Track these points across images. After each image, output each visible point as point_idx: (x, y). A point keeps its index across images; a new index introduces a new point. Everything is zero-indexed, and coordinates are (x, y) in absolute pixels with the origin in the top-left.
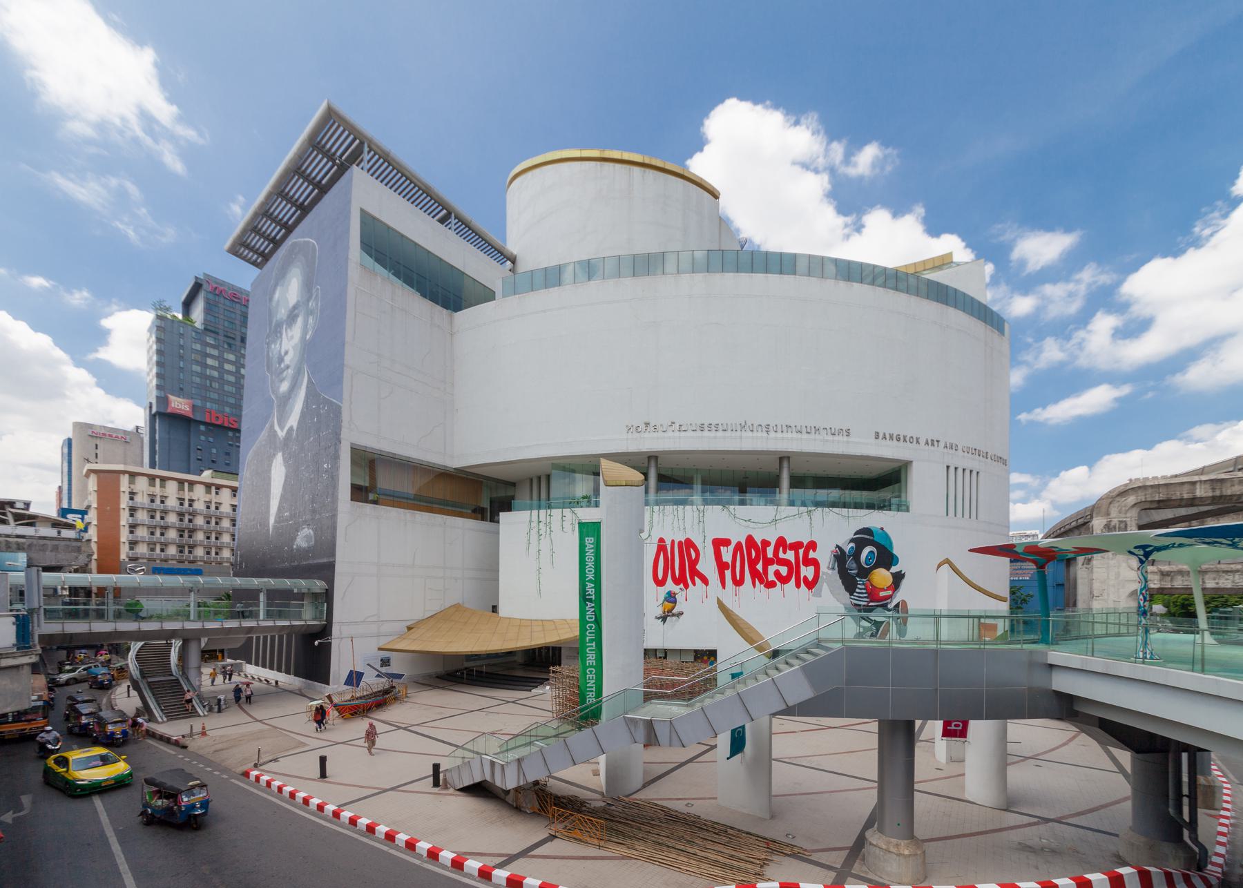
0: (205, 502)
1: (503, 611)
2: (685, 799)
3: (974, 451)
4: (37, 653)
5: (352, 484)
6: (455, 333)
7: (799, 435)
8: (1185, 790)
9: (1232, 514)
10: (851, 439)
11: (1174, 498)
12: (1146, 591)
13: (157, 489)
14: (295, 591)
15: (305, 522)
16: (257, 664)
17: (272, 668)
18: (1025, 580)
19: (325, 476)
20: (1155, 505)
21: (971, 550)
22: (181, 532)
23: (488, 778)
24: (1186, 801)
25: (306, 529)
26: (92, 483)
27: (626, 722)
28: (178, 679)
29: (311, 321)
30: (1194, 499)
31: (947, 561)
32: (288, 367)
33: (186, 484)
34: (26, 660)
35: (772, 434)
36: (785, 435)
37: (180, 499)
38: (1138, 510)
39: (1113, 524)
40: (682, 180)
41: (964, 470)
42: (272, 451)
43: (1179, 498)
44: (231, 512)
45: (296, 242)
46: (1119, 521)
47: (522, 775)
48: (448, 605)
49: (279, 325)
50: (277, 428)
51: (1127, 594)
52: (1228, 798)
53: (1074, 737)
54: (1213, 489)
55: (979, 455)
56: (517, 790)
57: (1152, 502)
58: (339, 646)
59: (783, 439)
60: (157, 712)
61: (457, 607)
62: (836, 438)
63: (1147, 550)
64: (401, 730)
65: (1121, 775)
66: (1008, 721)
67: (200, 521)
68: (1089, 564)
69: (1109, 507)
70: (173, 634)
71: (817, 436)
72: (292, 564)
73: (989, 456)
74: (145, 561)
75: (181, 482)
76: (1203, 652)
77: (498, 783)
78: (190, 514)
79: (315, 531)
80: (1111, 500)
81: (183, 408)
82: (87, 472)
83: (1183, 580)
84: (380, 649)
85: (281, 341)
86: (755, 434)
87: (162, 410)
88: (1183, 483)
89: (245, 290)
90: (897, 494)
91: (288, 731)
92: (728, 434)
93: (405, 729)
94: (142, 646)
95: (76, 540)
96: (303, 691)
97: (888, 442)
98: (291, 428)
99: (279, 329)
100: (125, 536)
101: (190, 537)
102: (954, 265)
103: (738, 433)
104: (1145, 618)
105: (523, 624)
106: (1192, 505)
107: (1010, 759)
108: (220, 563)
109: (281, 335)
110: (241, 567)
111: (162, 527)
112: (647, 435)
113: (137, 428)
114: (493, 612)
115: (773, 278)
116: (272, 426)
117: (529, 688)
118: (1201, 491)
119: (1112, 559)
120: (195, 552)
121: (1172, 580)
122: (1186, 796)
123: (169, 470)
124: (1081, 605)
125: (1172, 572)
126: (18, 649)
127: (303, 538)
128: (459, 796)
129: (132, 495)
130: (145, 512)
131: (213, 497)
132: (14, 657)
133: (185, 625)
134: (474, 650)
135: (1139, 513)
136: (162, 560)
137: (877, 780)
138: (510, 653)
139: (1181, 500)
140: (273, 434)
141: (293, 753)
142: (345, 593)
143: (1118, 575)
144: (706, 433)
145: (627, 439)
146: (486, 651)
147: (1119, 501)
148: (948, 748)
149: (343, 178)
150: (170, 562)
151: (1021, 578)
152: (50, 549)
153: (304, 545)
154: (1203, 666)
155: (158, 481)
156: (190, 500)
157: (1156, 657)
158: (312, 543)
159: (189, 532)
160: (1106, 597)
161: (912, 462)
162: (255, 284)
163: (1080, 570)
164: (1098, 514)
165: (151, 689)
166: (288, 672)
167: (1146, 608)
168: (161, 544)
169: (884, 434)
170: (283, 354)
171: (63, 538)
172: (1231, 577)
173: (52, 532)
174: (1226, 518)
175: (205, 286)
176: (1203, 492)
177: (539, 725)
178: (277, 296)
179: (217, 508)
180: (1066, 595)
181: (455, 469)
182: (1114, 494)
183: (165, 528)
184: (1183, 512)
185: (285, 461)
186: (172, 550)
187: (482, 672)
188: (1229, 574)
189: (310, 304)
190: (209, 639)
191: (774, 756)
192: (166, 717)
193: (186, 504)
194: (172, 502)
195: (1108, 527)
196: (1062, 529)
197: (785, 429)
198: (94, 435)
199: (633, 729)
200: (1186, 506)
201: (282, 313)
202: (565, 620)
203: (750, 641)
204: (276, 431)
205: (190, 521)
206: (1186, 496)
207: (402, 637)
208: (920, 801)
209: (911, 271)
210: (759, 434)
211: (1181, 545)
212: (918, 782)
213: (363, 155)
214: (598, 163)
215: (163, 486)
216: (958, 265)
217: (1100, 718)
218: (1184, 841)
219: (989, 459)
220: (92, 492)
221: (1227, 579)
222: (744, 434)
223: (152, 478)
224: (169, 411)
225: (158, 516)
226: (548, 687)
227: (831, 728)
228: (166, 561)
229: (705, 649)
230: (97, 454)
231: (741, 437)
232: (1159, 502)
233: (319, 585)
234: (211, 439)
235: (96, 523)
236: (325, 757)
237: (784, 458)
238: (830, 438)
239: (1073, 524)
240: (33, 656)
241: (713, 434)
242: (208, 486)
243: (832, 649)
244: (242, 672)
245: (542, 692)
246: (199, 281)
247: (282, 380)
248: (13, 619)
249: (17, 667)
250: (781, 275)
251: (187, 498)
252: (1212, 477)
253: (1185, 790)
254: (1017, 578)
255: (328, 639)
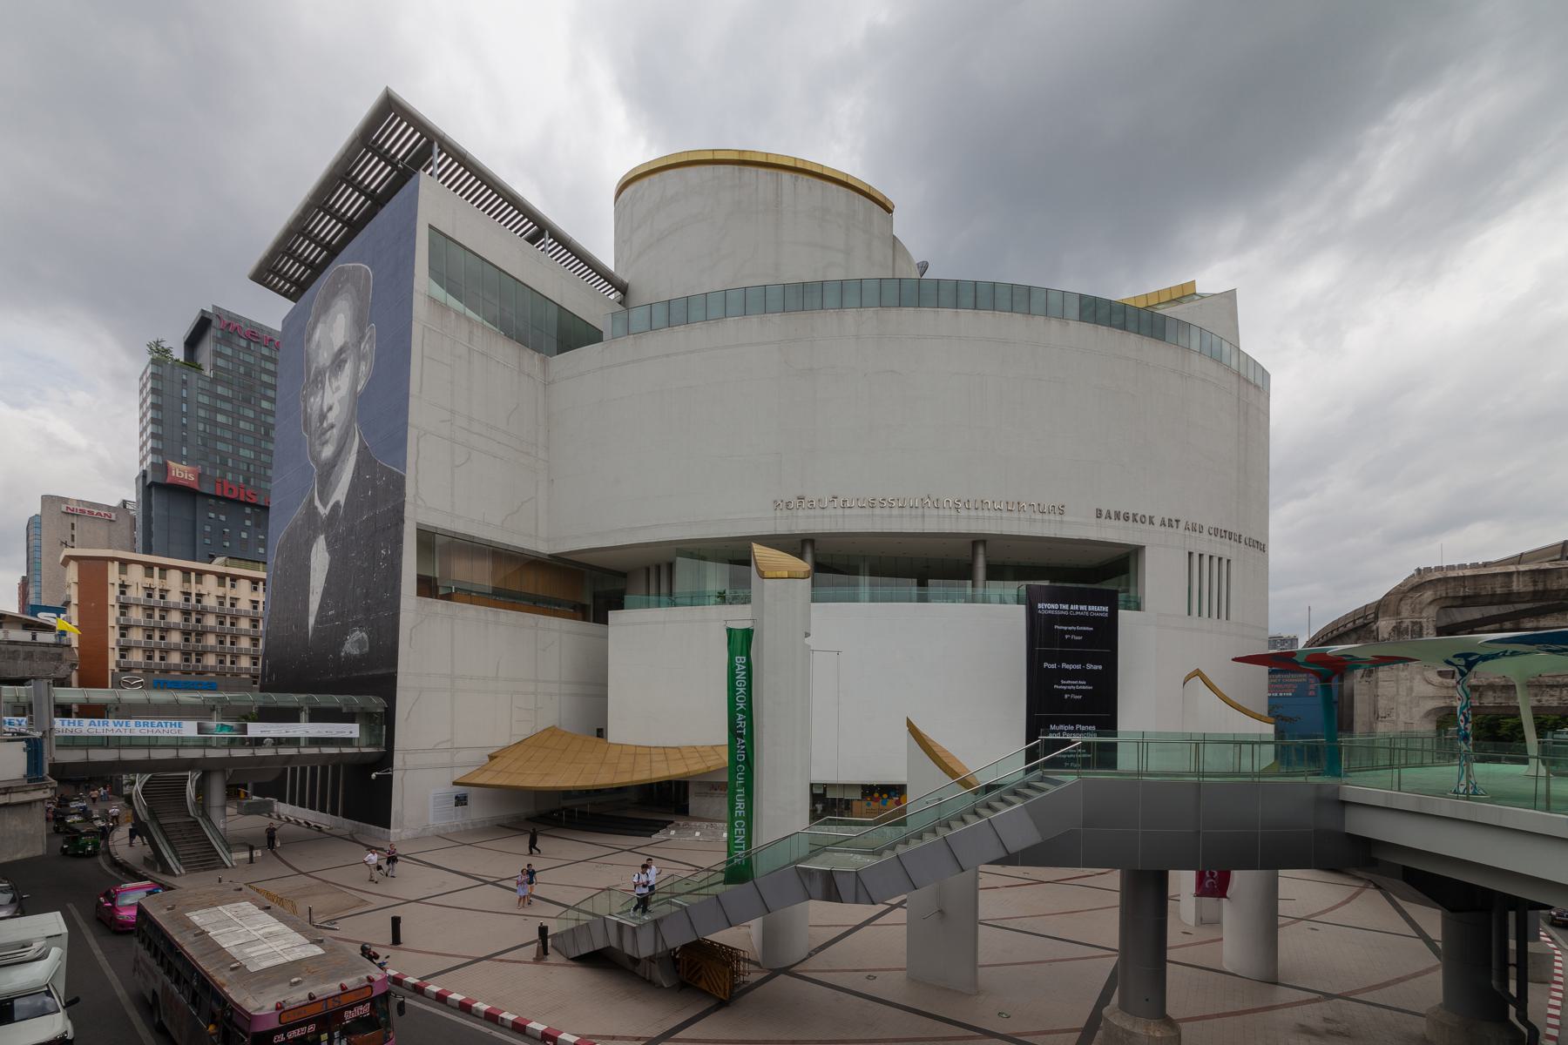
0: (218, 597)
1: (614, 735)
2: (865, 970)
3: (1223, 534)
4: (53, 786)
5: (418, 575)
6: (549, 383)
7: (999, 513)
8: (1513, 959)
9: (1556, 614)
10: (1066, 518)
11: (1483, 593)
12: (1468, 710)
13: (156, 582)
14: (344, 710)
15: (356, 623)
16: (292, 802)
17: (312, 807)
18: (1286, 696)
19: (383, 565)
20: (1459, 602)
21: (1236, 660)
22: (186, 634)
23: (614, 944)
24: (1513, 971)
25: (358, 632)
26: (72, 573)
27: (799, 874)
28: (197, 821)
29: (363, 368)
30: (1510, 594)
31: (1198, 673)
32: (332, 426)
33: (193, 575)
34: (39, 795)
35: (963, 512)
36: (980, 513)
37: (184, 593)
38: (1438, 608)
39: (1404, 625)
40: (846, 189)
41: (1211, 557)
42: (311, 532)
43: (1490, 593)
44: (251, 610)
45: (343, 267)
46: (1412, 622)
47: (660, 942)
48: (540, 728)
49: (320, 373)
50: (317, 503)
51: (1422, 714)
52: (1560, 972)
53: (1357, 894)
54: (1535, 583)
55: (1230, 539)
56: (651, 959)
57: (1455, 598)
58: (402, 779)
59: (977, 518)
60: (172, 862)
61: (552, 731)
62: (1046, 517)
63: (1470, 659)
64: (489, 886)
65: (1432, 938)
66: (1281, 872)
67: (211, 621)
68: (1370, 677)
69: (1399, 605)
70: (191, 764)
71: (1022, 515)
72: (340, 676)
73: (1243, 540)
74: (140, 672)
75: (186, 572)
76: (1548, 791)
77: (628, 950)
78: (198, 612)
79: (369, 634)
80: (1401, 596)
81: (186, 478)
82: (64, 559)
83: (1495, 697)
84: (455, 783)
85: (324, 393)
86: (941, 512)
87: (159, 480)
88: (1495, 575)
89: (266, 327)
90: (1124, 588)
91: (344, 886)
92: (906, 511)
93: (494, 884)
94: (149, 780)
95: (55, 645)
96: (355, 836)
97: (1113, 522)
98: (337, 503)
99: (319, 379)
100: (113, 637)
101: (198, 641)
102: (1197, 298)
103: (920, 511)
104: (1466, 744)
105: (638, 753)
106: (1507, 602)
107: (1281, 921)
108: (237, 675)
109: (323, 388)
110: (270, 680)
111: (162, 630)
112: (800, 513)
113: (124, 503)
114: (598, 736)
115: (966, 315)
116: (311, 501)
117: (649, 833)
118: (1518, 585)
119: (1403, 670)
120: (130, 656)
121: (1480, 697)
122: (1513, 965)
123: (168, 556)
124: (1359, 726)
125: (1479, 686)
126: (29, 781)
127: (355, 643)
128: (574, 966)
129: (124, 587)
130: (140, 609)
131: (229, 592)
132: (26, 792)
133: (232, 753)
134: (576, 785)
135: (1438, 611)
136: (162, 671)
137: (1117, 948)
138: (621, 790)
139: (1494, 595)
140: (312, 511)
141: (349, 914)
142: (409, 714)
143: (1411, 689)
144: (878, 511)
145: (775, 518)
146: (593, 786)
147: (1412, 597)
148: (1198, 908)
149: (405, 186)
150: (173, 673)
151: (1281, 694)
152: (22, 656)
153: (356, 652)
154: (1548, 802)
155: (156, 570)
156: (161, 590)
157: (1481, 791)
158: (367, 649)
159: (197, 635)
160: (1394, 718)
161: (1144, 547)
162: (287, 322)
163: (1357, 683)
164: (1385, 613)
165: (164, 833)
166: (334, 812)
167: (1468, 732)
168: (161, 650)
169: (1109, 512)
170: (325, 410)
171: (40, 643)
172: (1557, 693)
173: (26, 636)
174: (1548, 618)
175: (215, 322)
176: (1521, 586)
177: (677, 879)
178: (317, 335)
179: (232, 605)
180: (1339, 716)
181: (549, 555)
182: (1406, 588)
183: (166, 630)
184: (1494, 610)
185: (329, 545)
186: (175, 658)
187: (586, 813)
188: (1555, 689)
189: (362, 347)
190: (234, 771)
191: (981, 917)
192: (185, 868)
193: (193, 599)
194: (175, 597)
195: (1398, 630)
196: (1335, 632)
197: (978, 504)
198: (69, 511)
199: (807, 883)
200: (1500, 603)
201: (324, 358)
202: (695, 747)
203: (952, 773)
204: (316, 508)
205: (198, 621)
206: (1499, 591)
207: (482, 769)
208: (1174, 975)
209: (1142, 305)
210: (947, 512)
211: (1514, 654)
212: (1171, 948)
213: (432, 158)
214: (736, 167)
215: (199, 582)
216: (1203, 297)
217: (1404, 866)
218: (1510, 1021)
219: (1243, 542)
220: (72, 585)
221: (1552, 696)
222: (927, 511)
223: (149, 567)
224: (168, 481)
225: (157, 614)
226: (673, 832)
227: (1043, 882)
228: (167, 671)
229: (875, 783)
230: (73, 536)
231: (923, 516)
232: (1464, 598)
233: (376, 703)
234: (223, 518)
235: (77, 624)
236: (399, 918)
237: (978, 541)
238: (1039, 516)
239: (1348, 625)
240: (48, 790)
241: (886, 512)
242: (221, 577)
243: (1064, 782)
244: (273, 812)
245: (665, 838)
246: (207, 316)
247: (324, 443)
248: (24, 744)
249: (29, 803)
250: (976, 311)
251: (194, 592)
252: (1534, 566)
253: (1513, 959)
254: (1276, 695)
255: (389, 771)
